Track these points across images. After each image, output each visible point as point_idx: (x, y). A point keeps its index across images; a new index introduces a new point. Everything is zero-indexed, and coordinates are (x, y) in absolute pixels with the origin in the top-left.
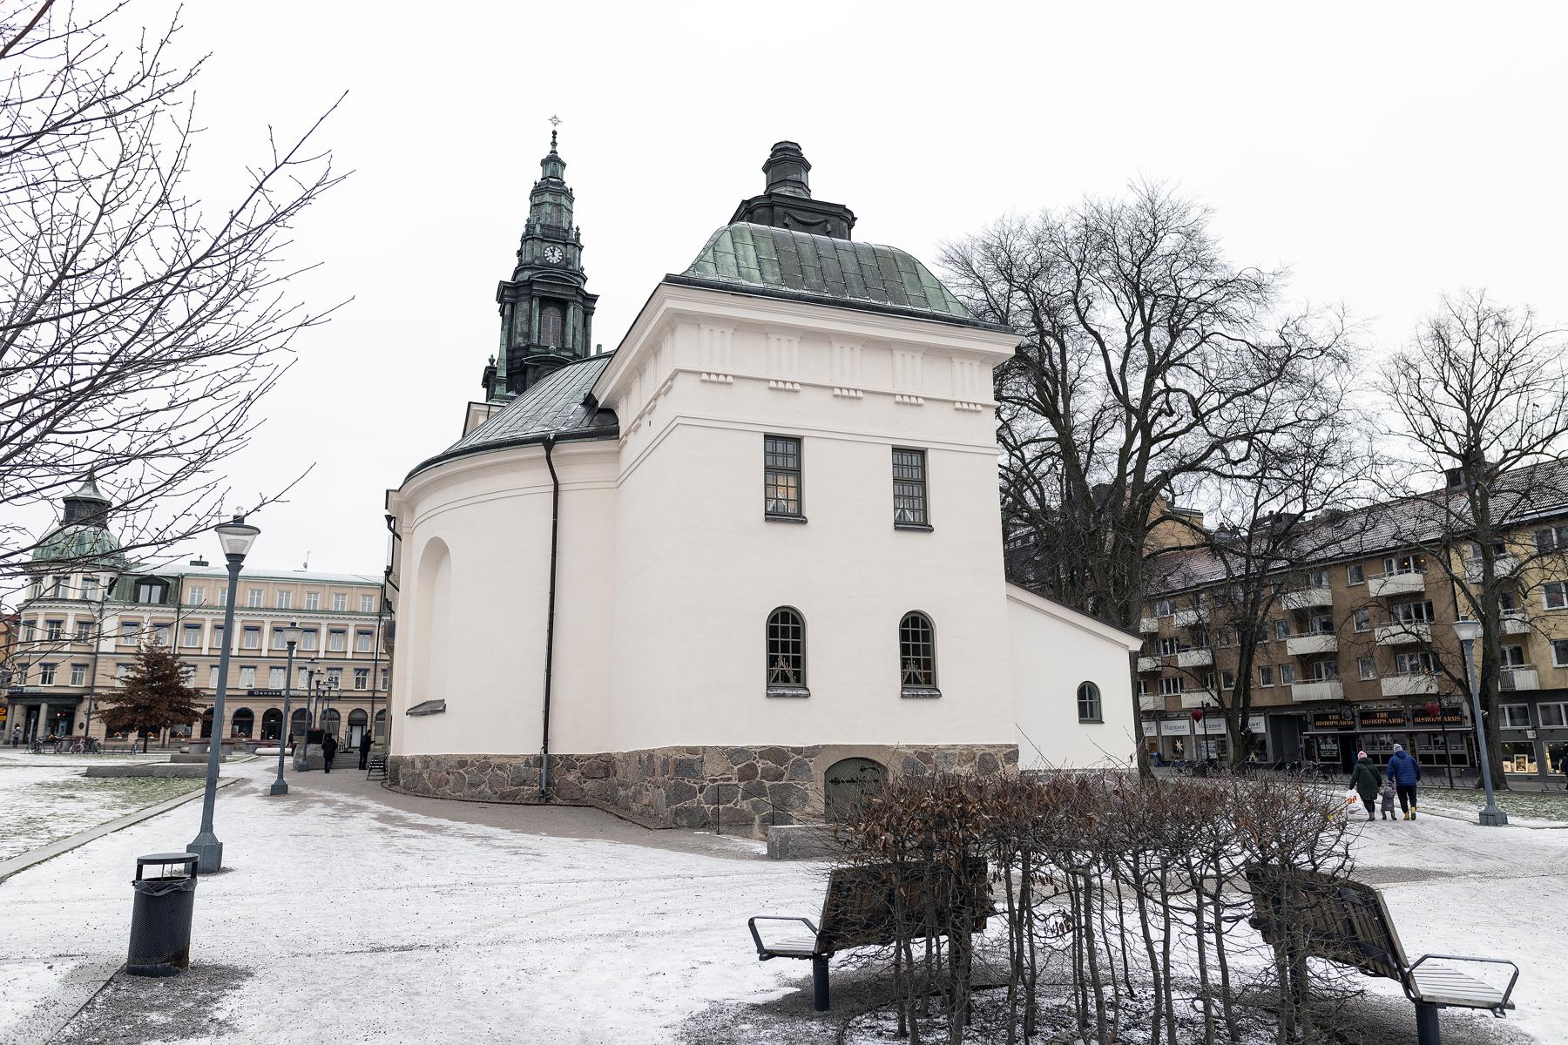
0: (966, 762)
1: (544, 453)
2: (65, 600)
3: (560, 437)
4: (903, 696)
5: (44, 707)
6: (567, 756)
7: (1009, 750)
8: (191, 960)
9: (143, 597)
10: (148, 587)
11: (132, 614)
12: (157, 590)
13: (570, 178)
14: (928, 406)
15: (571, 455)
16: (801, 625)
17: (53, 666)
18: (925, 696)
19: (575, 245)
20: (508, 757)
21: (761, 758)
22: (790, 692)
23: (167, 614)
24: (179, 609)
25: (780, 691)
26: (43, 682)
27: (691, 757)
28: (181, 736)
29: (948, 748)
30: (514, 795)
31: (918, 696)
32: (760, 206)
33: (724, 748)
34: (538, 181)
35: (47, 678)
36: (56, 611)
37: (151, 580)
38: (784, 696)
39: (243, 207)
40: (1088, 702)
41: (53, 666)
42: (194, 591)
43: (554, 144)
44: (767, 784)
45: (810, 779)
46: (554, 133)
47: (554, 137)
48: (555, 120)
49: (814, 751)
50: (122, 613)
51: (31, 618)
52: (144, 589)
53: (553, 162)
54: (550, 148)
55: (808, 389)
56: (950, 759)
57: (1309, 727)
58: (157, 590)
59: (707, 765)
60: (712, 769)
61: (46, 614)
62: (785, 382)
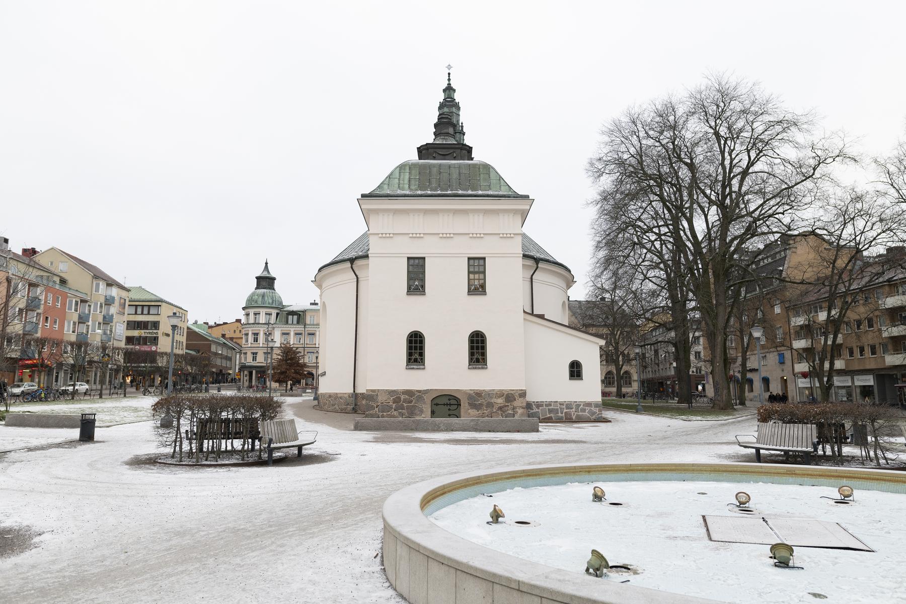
0: (499, 397)
1: (350, 265)
2: (259, 324)
3: (357, 258)
4: (469, 368)
5: (254, 372)
6: (363, 393)
7: (521, 392)
8: (79, 429)
9: (290, 321)
10: (292, 316)
11: (286, 328)
12: (295, 317)
13: (457, 97)
14: (487, 237)
15: (363, 265)
16: (423, 339)
17: (256, 353)
18: (480, 368)
19: (460, 133)
20: (343, 393)
21: (403, 394)
22: (417, 367)
23: (300, 328)
24: (305, 326)
25: (412, 367)
26: (253, 361)
27: (373, 393)
28: (310, 385)
29: (491, 391)
30: (346, 409)
31: (476, 368)
32: (424, 149)
33: (387, 390)
34: (442, 101)
35: (254, 359)
36: (256, 329)
37: (293, 313)
38: (413, 368)
39: (42, 448)
40: (575, 370)
41: (256, 353)
42: (311, 317)
43: (449, 80)
44: (405, 405)
45: (425, 403)
46: (449, 74)
47: (449, 76)
48: (449, 67)
49: (426, 392)
50: (282, 329)
51: (246, 332)
52: (290, 317)
53: (449, 90)
54: (447, 82)
55: (428, 236)
56: (491, 395)
57: (899, 381)
58: (295, 317)
59: (379, 396)
60: (381, 398)
61: (252, 330)
62: (416, 234)
